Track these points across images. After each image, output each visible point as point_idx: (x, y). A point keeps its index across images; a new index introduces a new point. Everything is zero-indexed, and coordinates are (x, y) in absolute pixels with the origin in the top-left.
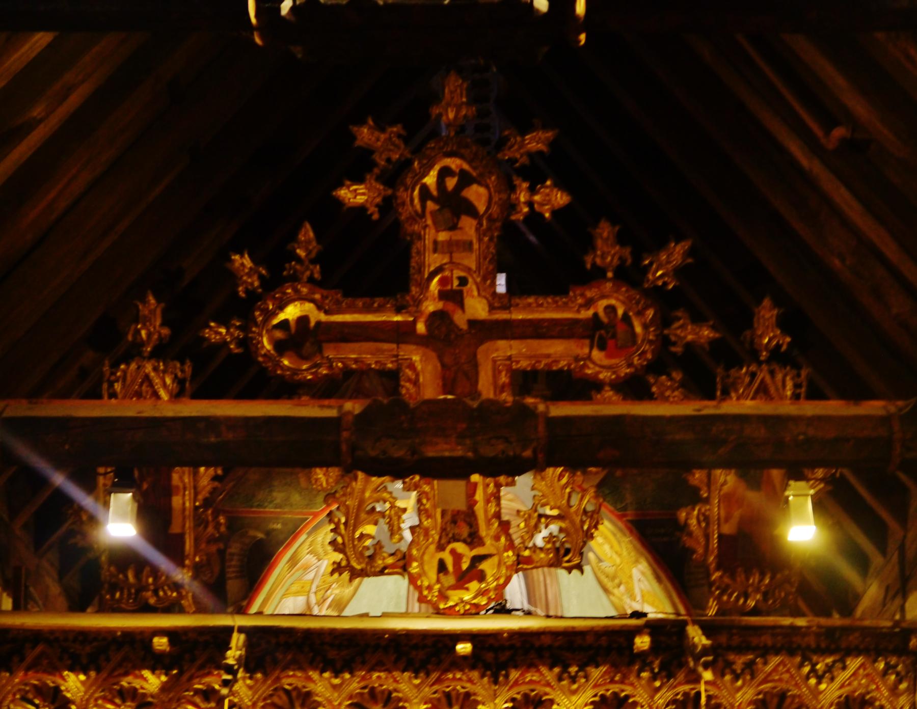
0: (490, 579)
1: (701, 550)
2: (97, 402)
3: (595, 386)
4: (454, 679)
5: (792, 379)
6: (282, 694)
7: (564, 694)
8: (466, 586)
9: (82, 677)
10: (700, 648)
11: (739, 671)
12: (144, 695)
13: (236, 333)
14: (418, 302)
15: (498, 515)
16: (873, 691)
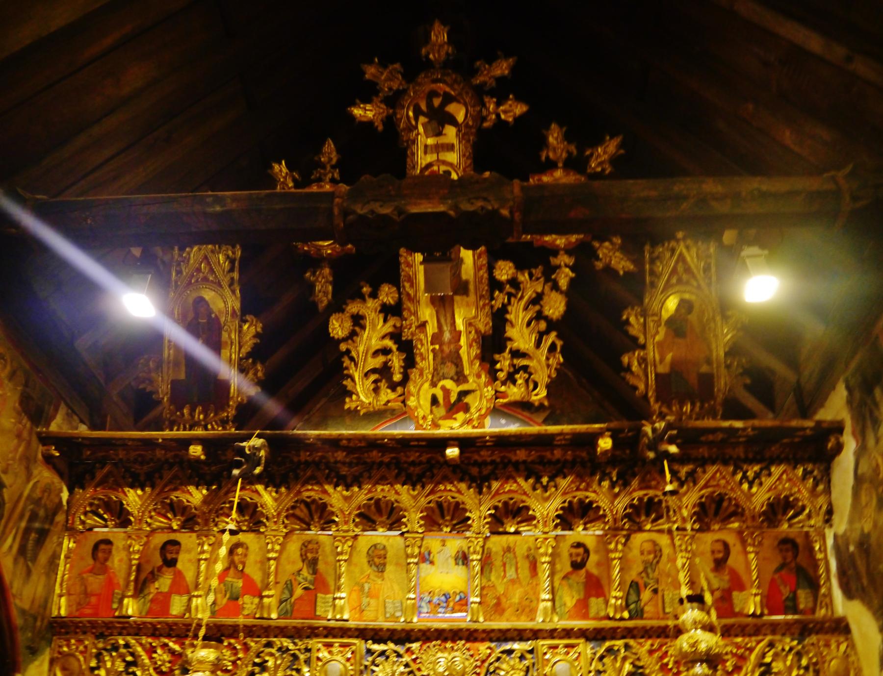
0: (473, 410)
4: (445, 490)
6: (302, 506)
7: (538, 501)
8: (454, 416)
9: (139, 492)
11: (683, 479)
16: (795, 493)
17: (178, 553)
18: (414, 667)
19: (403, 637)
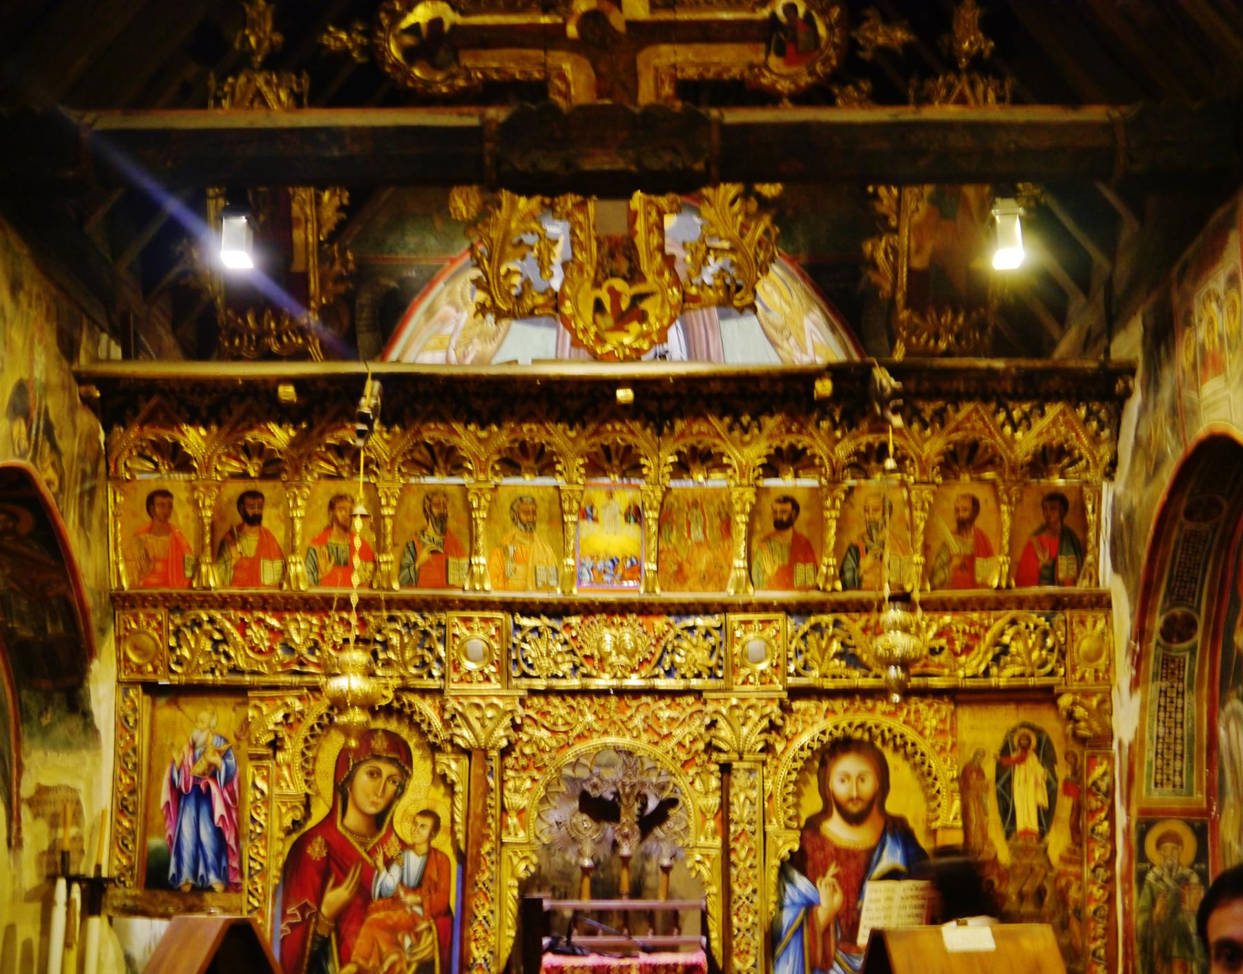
0: (652, 319)
1: (887, 287)
2: (201, 112)
3: (768, 98)
5: (995, 90)
10: (889, 390)
11: (928, 419)
12: (273, 451)
13: (359, 39)
15: (661, 248)
18: (573, 644)
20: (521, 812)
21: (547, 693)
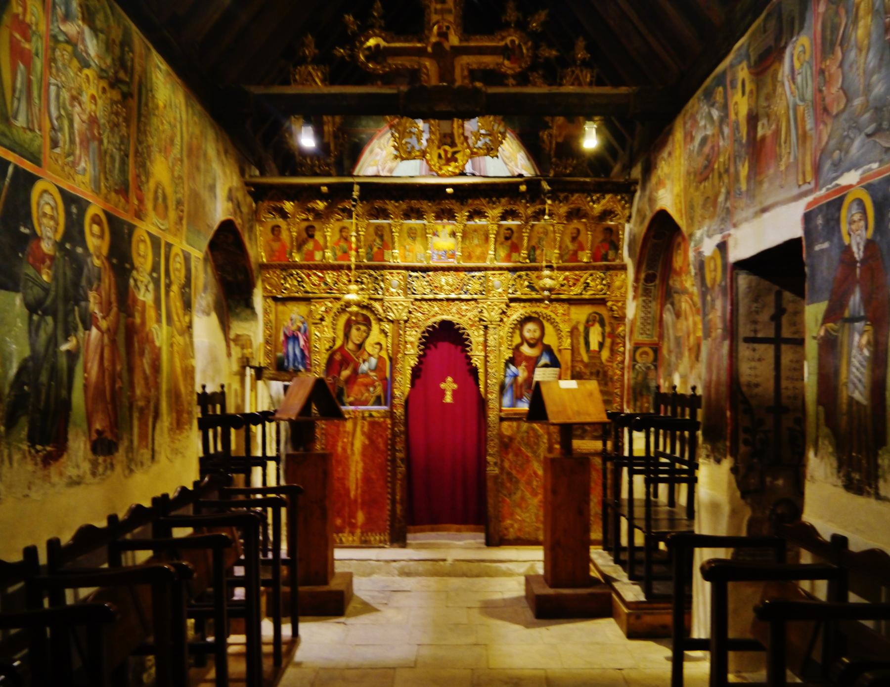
0: (459, 161)
9: (292, 203)
14: (428, 38)
15: (463, 134)
17: (314, 231)
19: (425, 270)
20: (412, 343)
21: (420, 300)
